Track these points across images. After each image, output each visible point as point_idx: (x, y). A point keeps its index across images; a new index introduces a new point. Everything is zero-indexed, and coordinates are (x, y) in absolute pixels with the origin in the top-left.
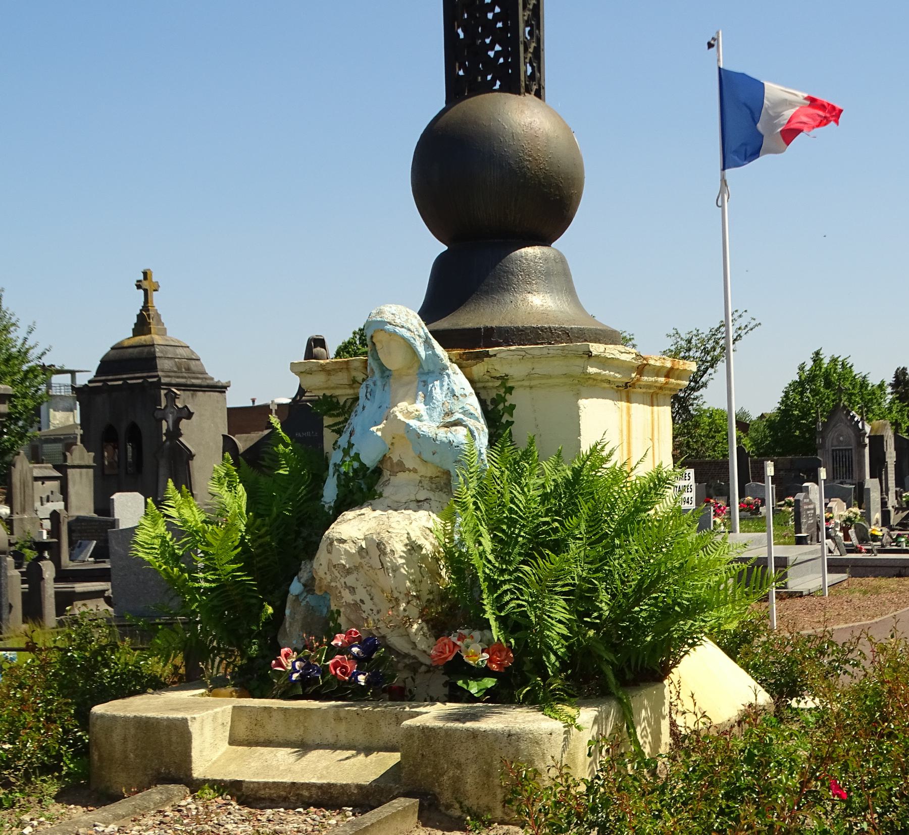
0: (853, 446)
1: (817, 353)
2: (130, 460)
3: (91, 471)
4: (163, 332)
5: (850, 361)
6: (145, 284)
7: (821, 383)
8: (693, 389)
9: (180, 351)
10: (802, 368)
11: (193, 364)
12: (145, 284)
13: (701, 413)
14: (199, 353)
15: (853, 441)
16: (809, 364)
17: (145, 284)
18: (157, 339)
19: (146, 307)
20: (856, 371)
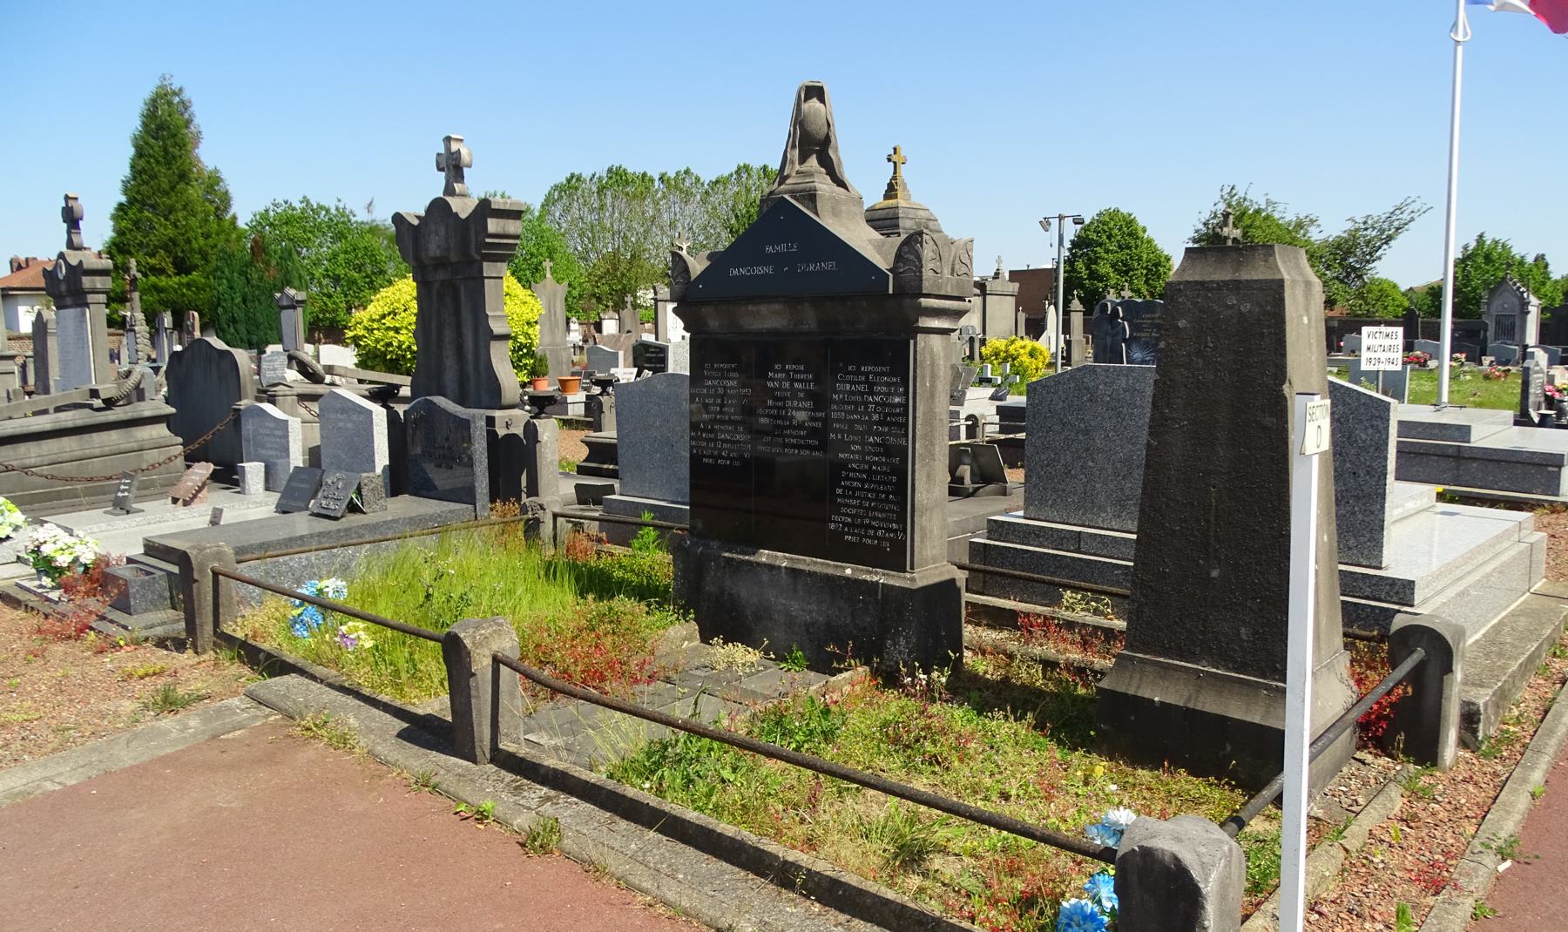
0: (1517, 312)
1: (1481, 236)
2: (801, 268)
3: (1012, 300)
4: (908, 198)
5: (1510, 243)
6: (894, 159)
7: (1480, 260)
8: (1368, 262)
9: (921, 213)
10: (1465, 248)
11: (931, 224)
12: (894, 159)
13: (1373, 281)
14: (936, 215)
15: (1518, 308)
16: (1473, 245)
17: (894, 158)
18: (901, 202)
19: (894, 178)
20: (1514, 251)
